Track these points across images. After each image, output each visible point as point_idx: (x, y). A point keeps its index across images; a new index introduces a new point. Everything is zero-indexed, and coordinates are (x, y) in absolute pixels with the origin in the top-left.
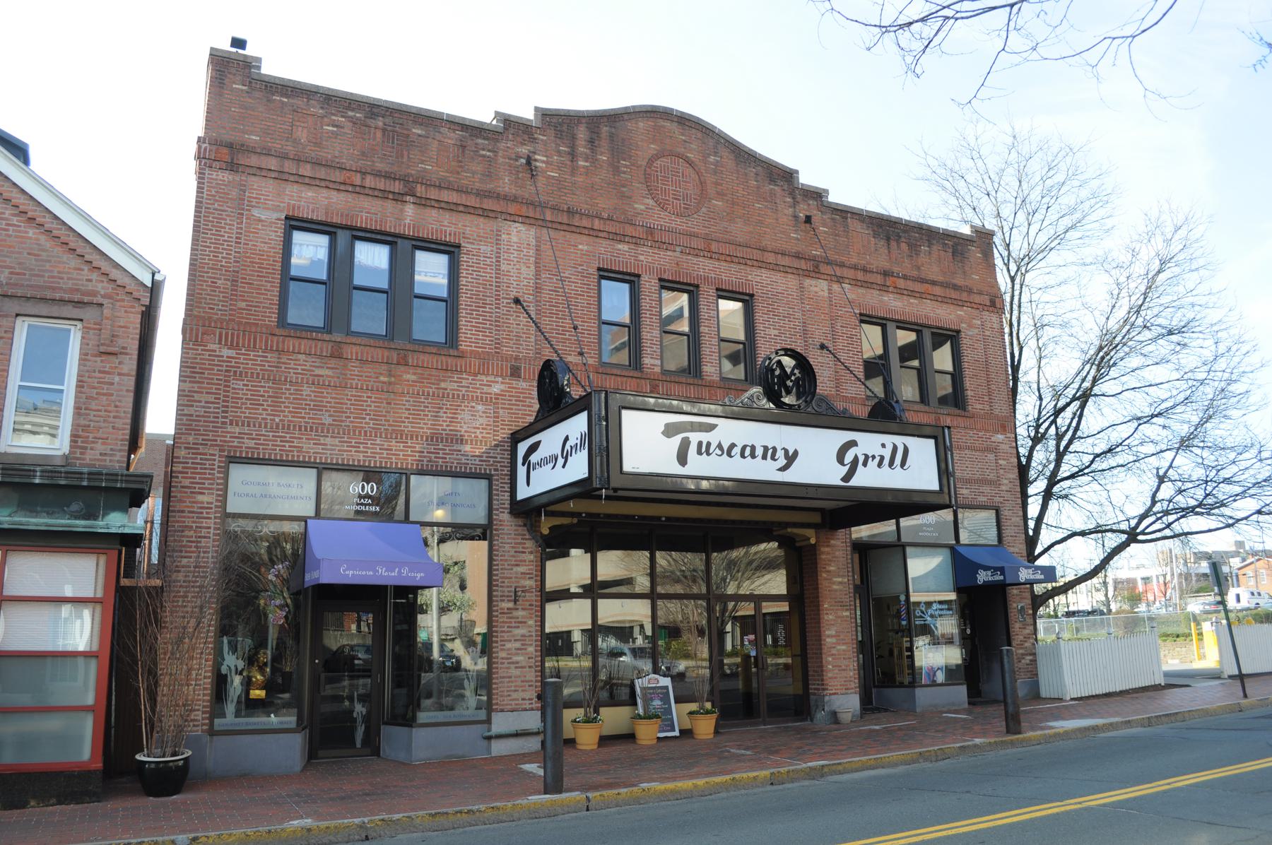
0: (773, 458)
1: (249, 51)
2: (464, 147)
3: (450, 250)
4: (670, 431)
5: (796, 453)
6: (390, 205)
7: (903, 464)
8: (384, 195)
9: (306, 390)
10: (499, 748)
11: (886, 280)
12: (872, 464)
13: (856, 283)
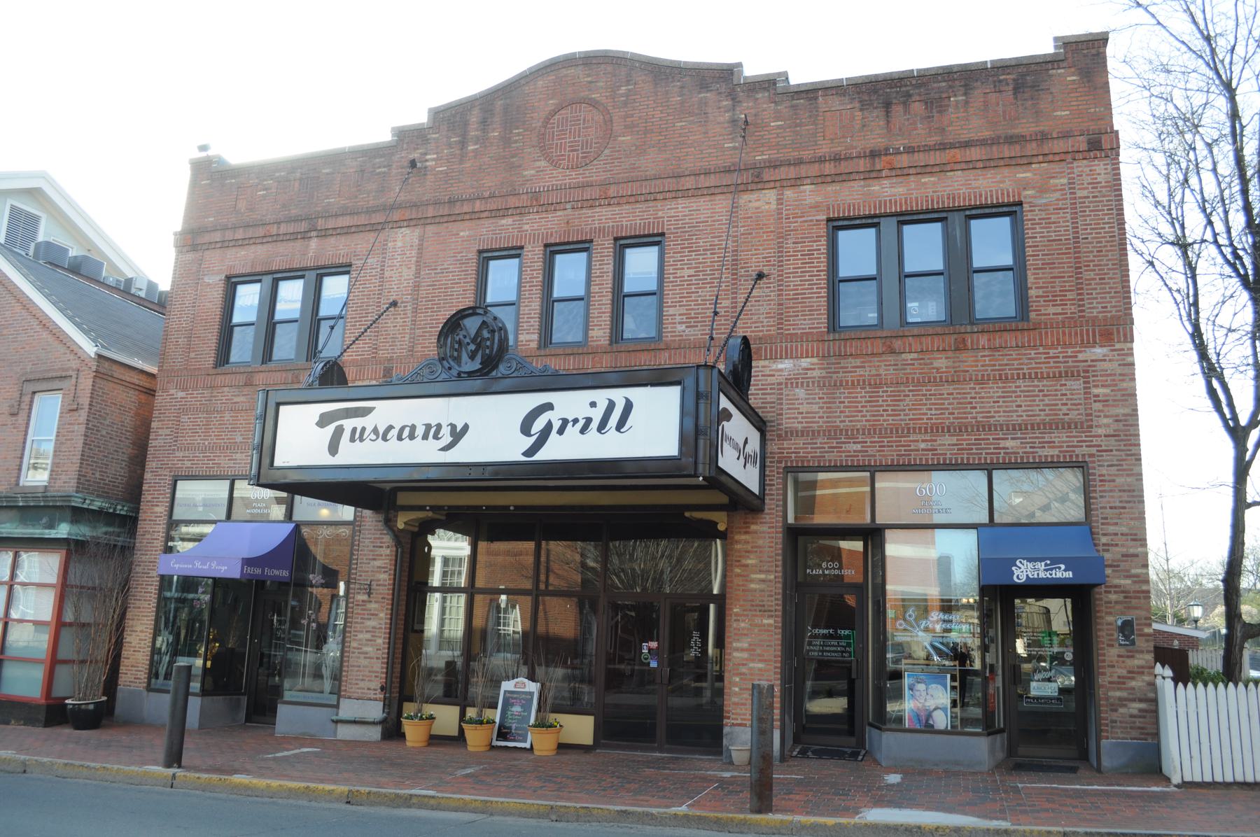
0: (436, 437)
1: (210, 153)
2: (363, 171)
3: (1010, 209)
4: (324, 421)
5: (466, 428)
6: (299, 244)
7: (619, 427)
8: (294, 236)
9: (227, 416)
10: (345, 732)
11: (876, 162)
13: (822, 180)
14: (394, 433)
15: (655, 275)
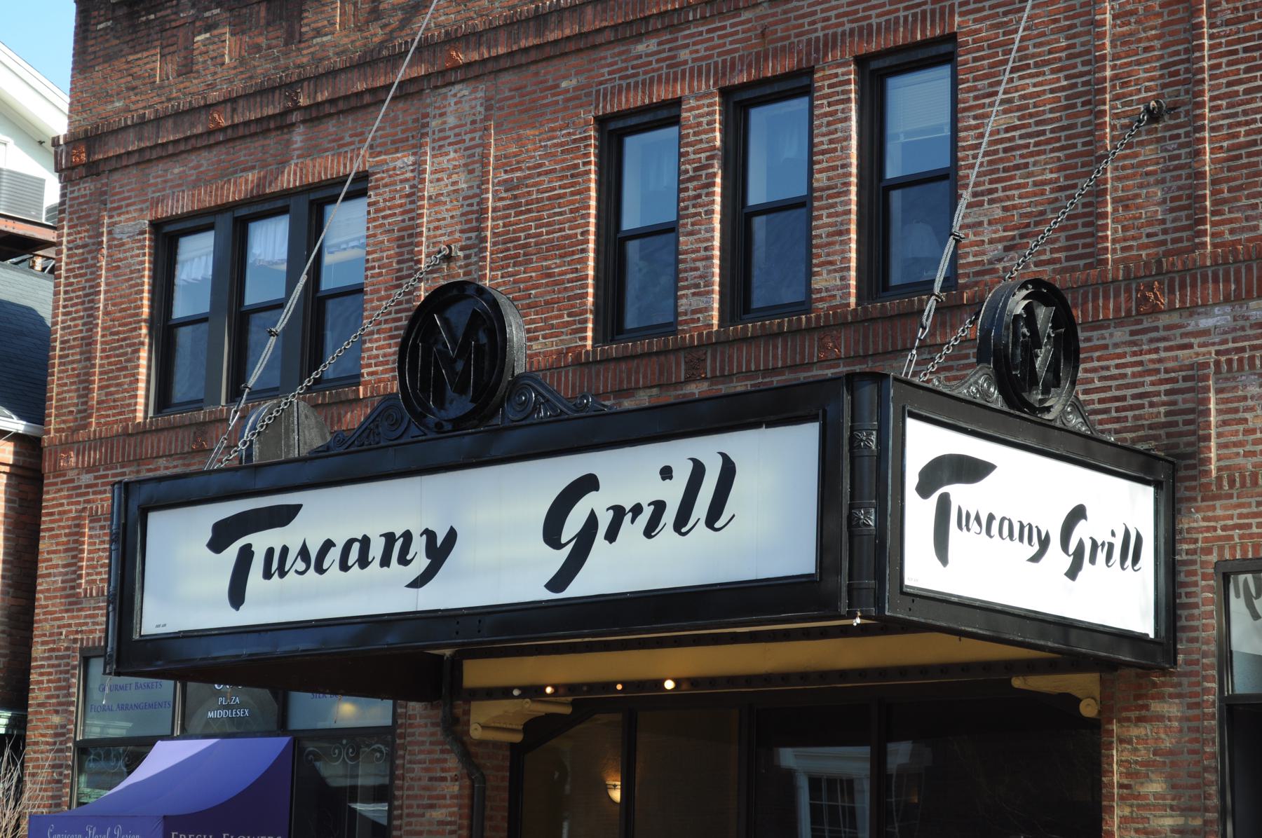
0: (403, 561)
5: (452, 536)
12: (631, 531)
14: (334, 555)
15: (947, 132)
